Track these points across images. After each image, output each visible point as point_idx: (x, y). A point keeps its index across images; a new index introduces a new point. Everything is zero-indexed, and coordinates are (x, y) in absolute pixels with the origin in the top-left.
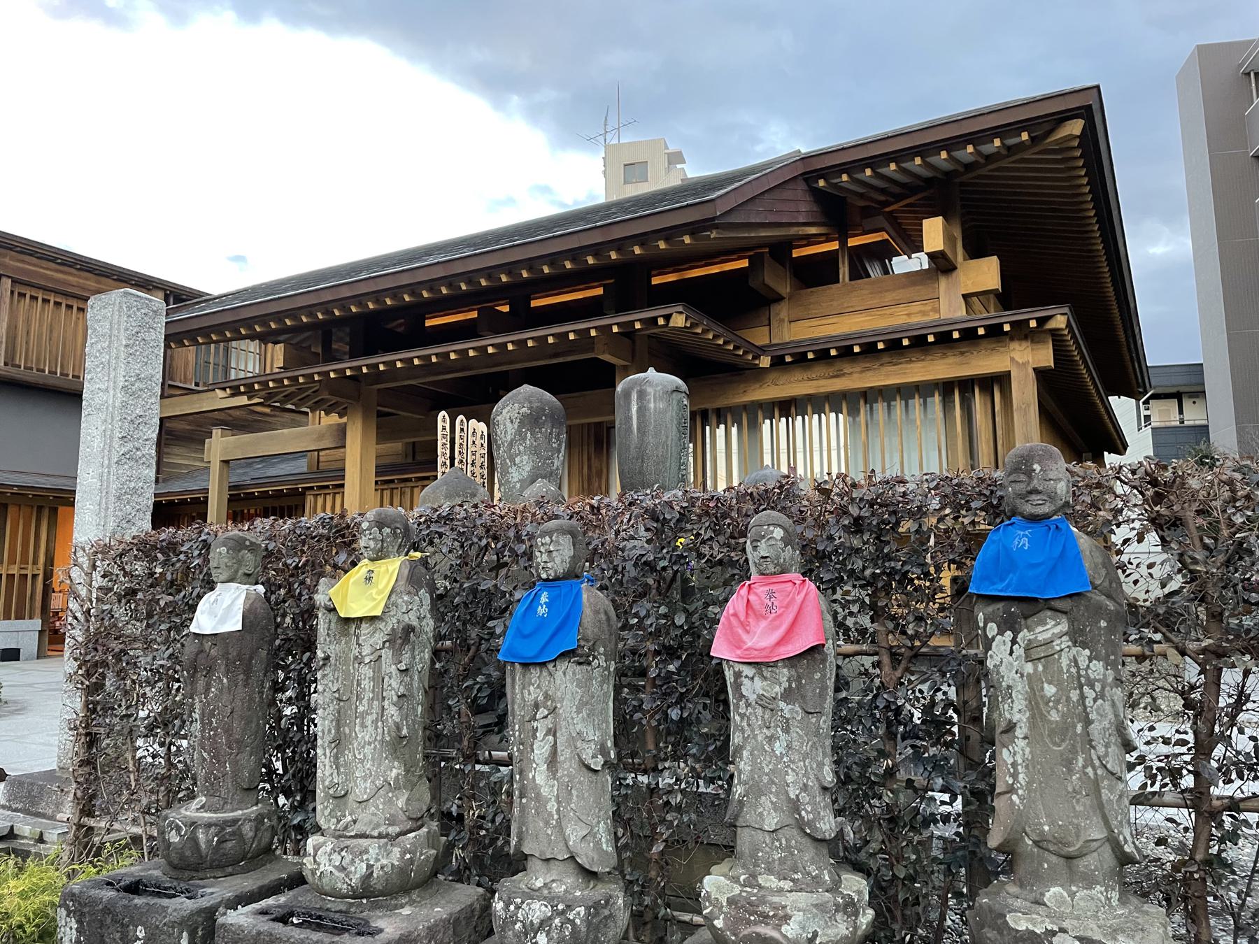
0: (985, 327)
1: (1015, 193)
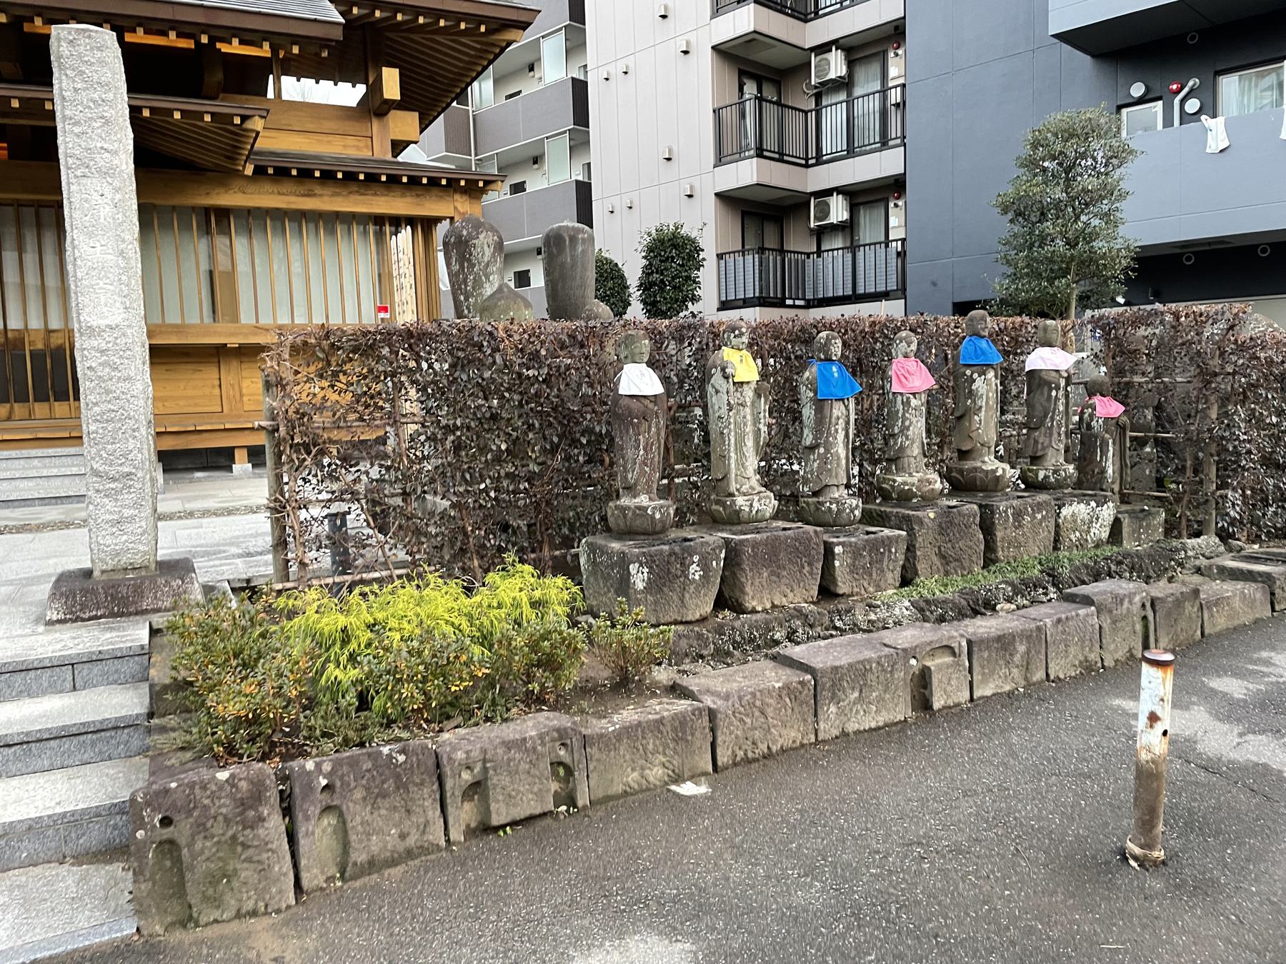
0: (448, 179)
1: (405, 53)
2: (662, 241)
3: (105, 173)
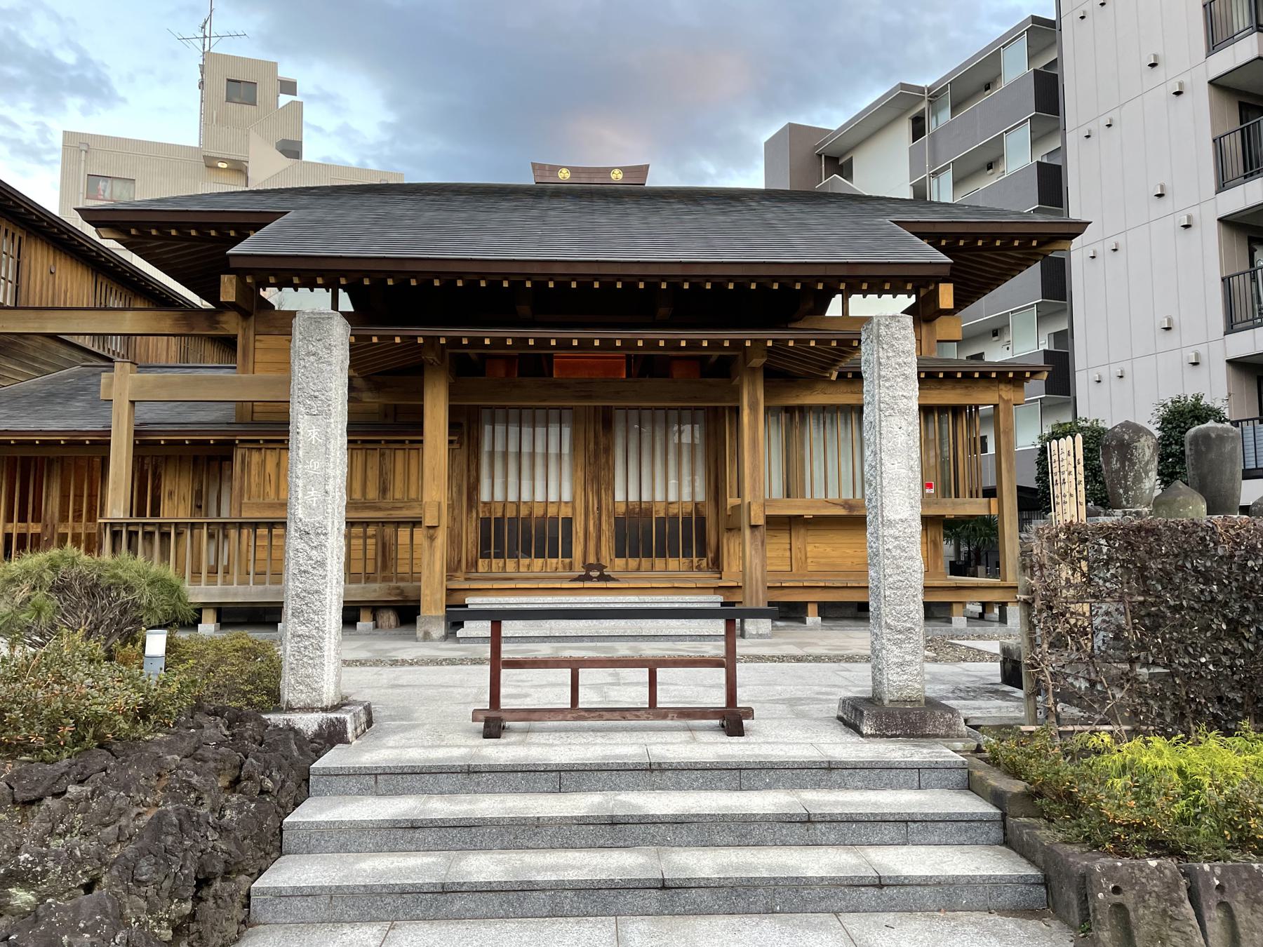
2: (1181, 414)
3: (903, 413)
